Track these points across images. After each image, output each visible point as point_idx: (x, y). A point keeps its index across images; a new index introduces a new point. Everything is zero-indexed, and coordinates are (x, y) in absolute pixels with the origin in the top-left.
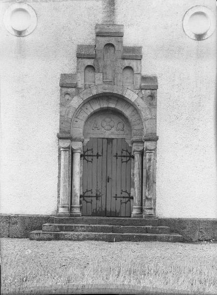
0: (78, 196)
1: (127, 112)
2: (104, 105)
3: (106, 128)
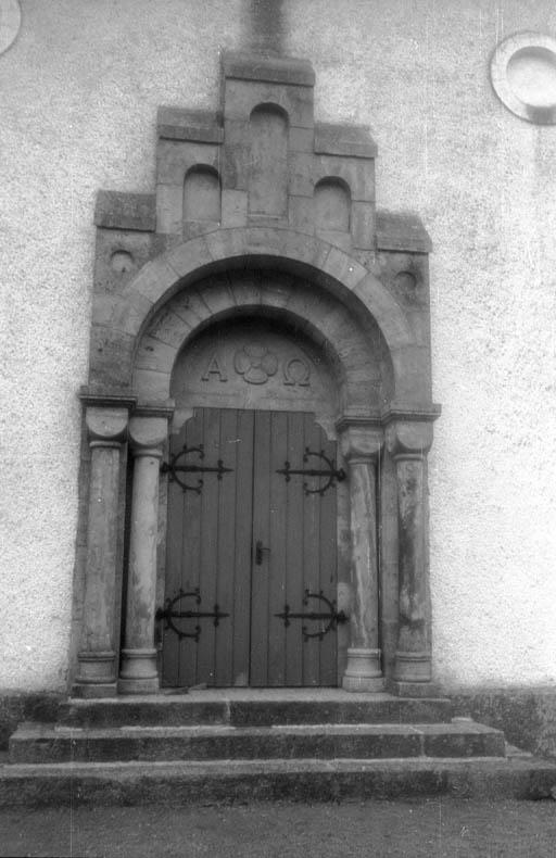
0: (148, 617)
1: (327, 325)
2: (248, 298)
3: (251, 375)
